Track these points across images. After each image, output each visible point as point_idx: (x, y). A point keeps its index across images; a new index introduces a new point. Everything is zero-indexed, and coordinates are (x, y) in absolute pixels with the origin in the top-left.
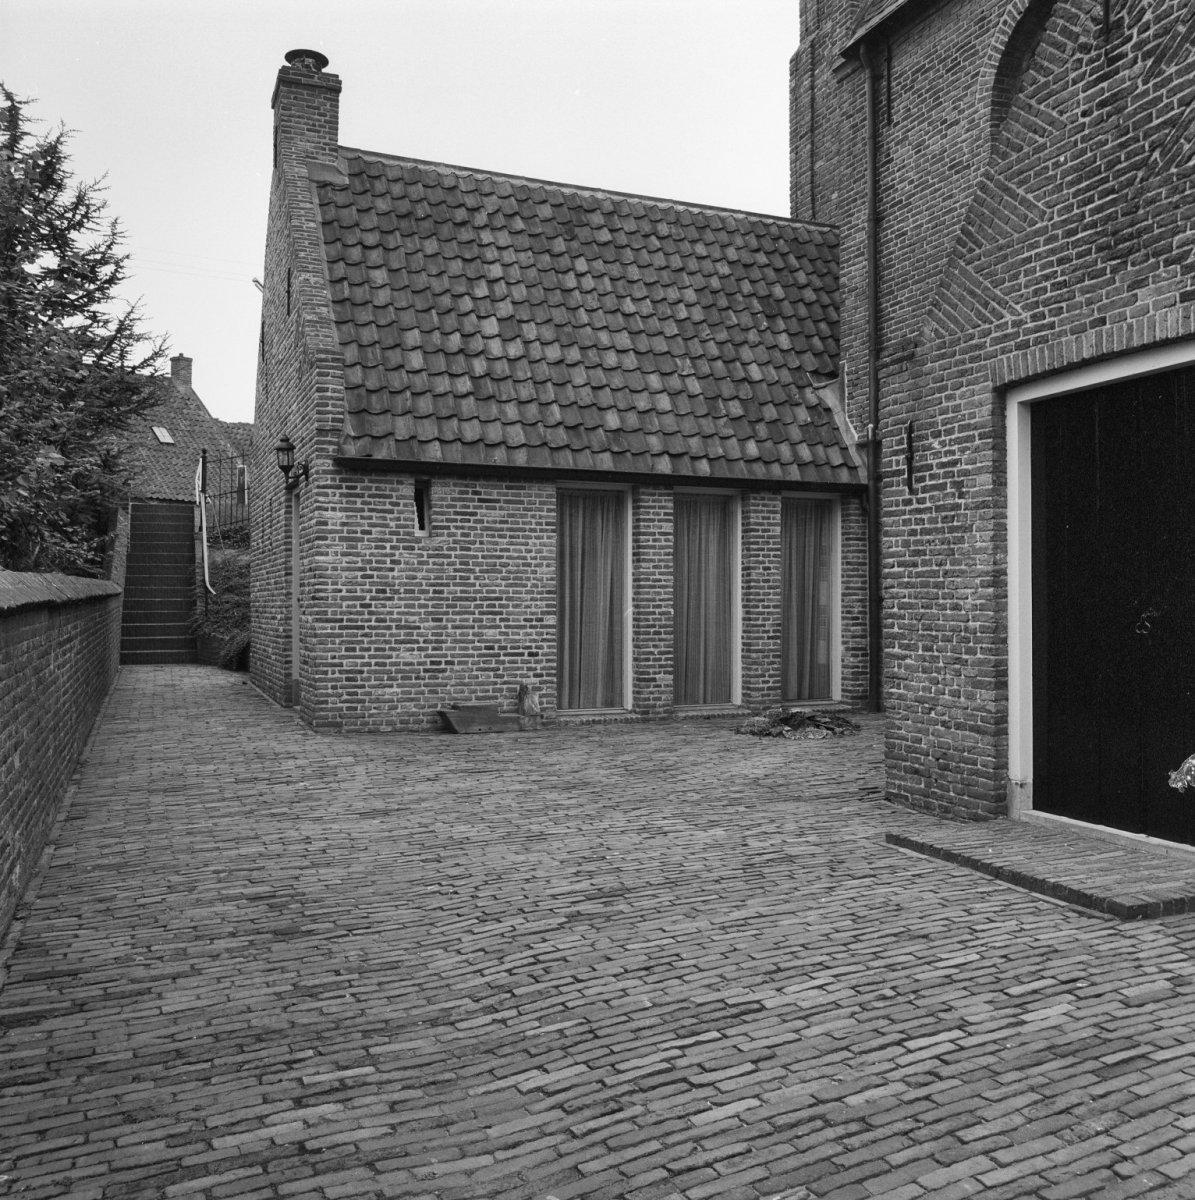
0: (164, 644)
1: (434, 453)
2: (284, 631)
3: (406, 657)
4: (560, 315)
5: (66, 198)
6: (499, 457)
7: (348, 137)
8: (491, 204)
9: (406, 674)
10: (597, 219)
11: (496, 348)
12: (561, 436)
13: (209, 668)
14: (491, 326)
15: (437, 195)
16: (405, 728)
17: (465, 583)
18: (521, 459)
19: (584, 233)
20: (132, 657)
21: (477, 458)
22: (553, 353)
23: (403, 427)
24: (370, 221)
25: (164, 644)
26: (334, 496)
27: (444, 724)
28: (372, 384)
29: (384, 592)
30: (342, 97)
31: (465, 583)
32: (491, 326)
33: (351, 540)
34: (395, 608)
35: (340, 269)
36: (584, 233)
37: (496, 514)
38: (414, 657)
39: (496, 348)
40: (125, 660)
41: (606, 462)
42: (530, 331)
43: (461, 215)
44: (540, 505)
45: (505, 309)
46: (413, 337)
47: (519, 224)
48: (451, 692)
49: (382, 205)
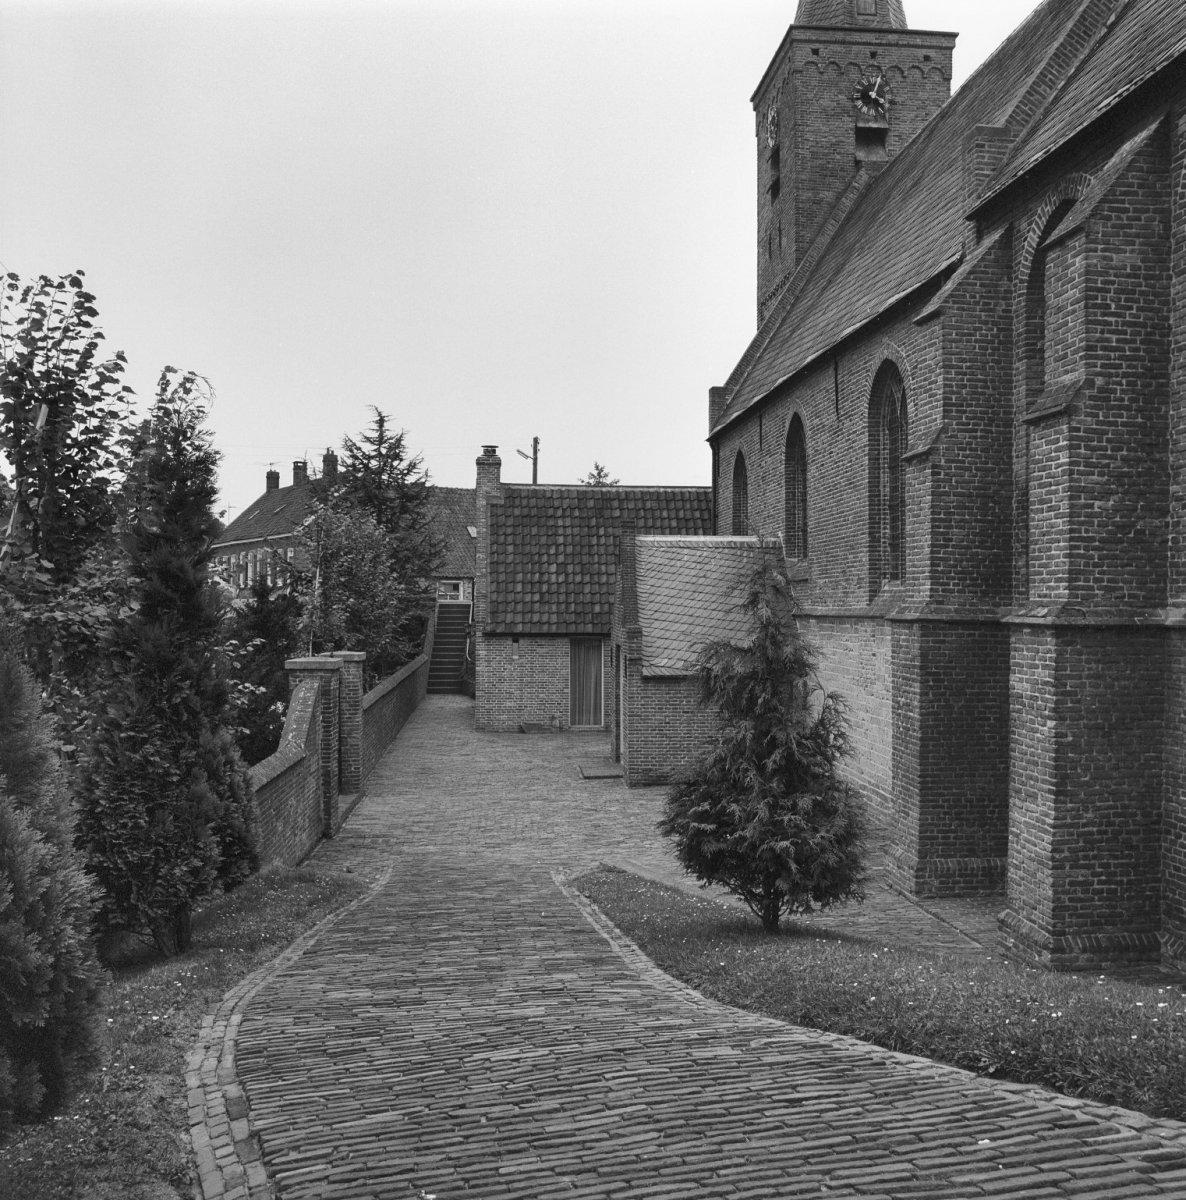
0: (449, 684)
1: (519, 628)
2: (939, 474)
3: (509, 704)
4: (585, 559)
5: (403, 465)
6: (545, 629)
7: (504, 479)
8: (566, 504)
9: (509, 710)
10: (616, 504)
11: (553, 578)
12: (573, 617)
13: (465, 698)
14: (553, 568)
15: (541, 503)
16: (509, 731)
17: (532, 676)
18: (554, 629)
19: (607, 513)
20: (433, 690)
21: (535, 630)
22: (578, 578)
23: (509, 618)
24: (510, 521)
25: (449, 684)
26: (483, 645)
27: (521, 730)
28: (500, 599)
29: (501, 680)
30: (502, 469)
31: (532, 676)
32: (553, 568)
33: (489, 661)
34: (505, 686)
35: (495, 547)
36: (607, 513)
37: (544, 650)
38: (512, 704)
39: (553, 578)
40: (430, 692)
41: (589, 628)
42: (570, 568)
43: (551, 512)
44: (564, 647)
45: (561, 558)
46: (520, 577)
47: (577, 513)
48: (526, 718)
49: (517, 512)
